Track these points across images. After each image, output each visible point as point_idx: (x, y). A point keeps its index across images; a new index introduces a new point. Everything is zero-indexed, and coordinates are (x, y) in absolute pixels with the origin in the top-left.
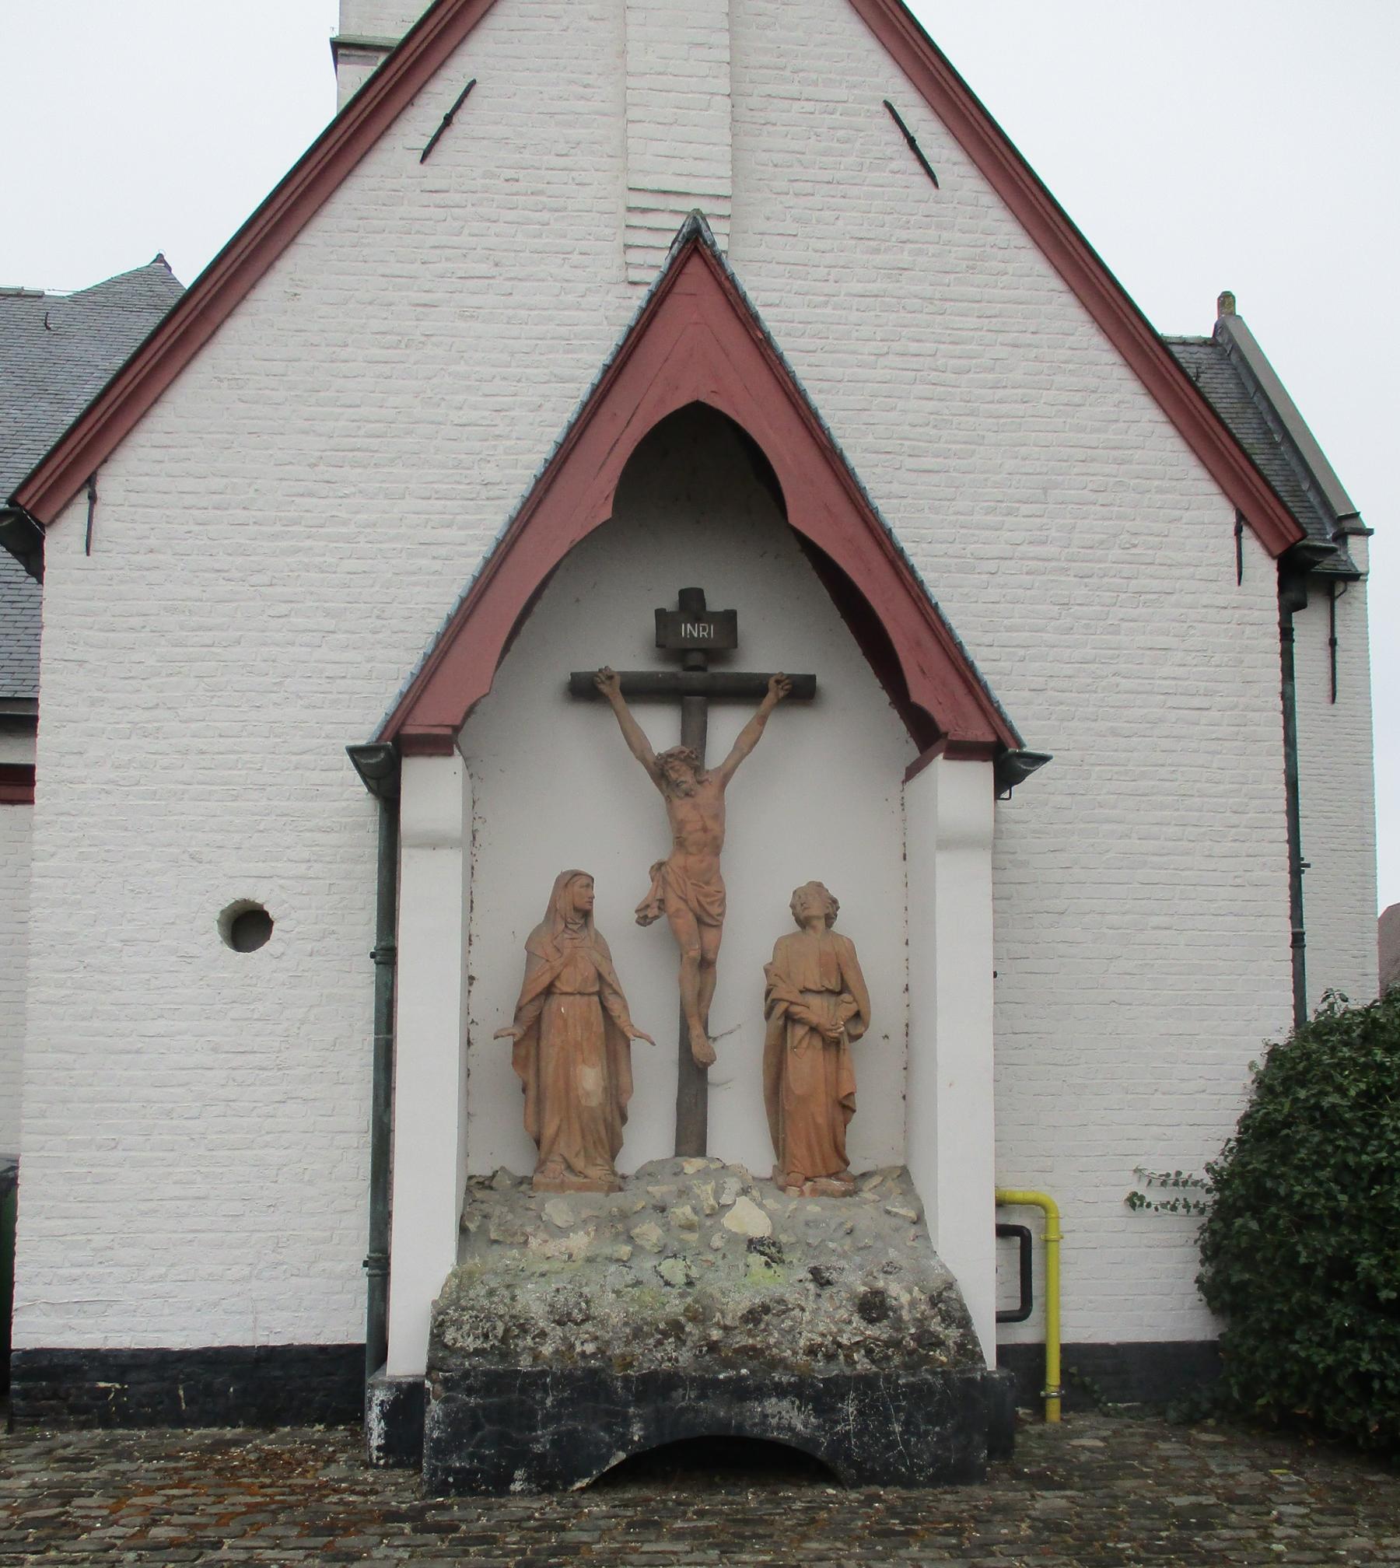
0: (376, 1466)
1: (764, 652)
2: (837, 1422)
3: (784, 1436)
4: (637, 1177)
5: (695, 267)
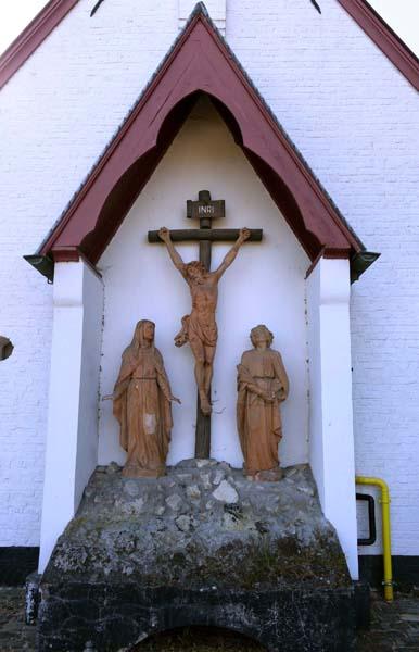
0: (28, 624)
1: (239, 218)
2: (268, 619)
3: (237, 627)
4: (175, 468)
5: (200, 27)
